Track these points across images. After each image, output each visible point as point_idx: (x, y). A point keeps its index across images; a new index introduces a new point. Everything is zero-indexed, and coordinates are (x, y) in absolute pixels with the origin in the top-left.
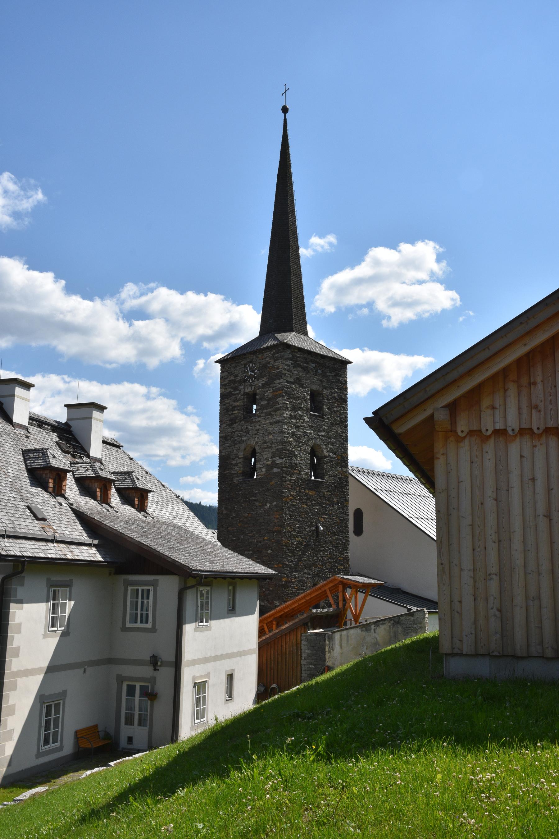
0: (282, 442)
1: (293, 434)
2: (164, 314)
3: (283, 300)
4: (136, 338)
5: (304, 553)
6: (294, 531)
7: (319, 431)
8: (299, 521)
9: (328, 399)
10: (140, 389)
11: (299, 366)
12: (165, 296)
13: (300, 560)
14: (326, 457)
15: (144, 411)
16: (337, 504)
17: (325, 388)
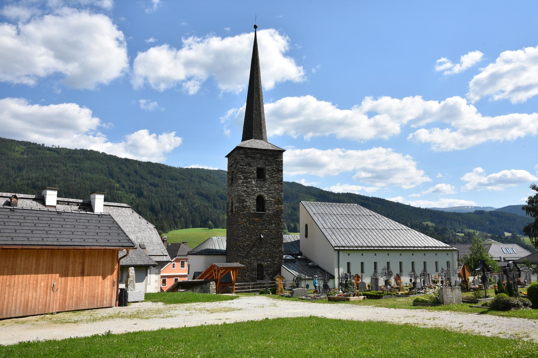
0: (238, 196)
1: (245, 191)
2: (388, 111)
3: (253, 124)
4: (376, 125)
5: (251, 249)
6: (245, 238)
7: (263, 188)
8: (248, 234)
9: (269, 171)
10: (381, 150)
11: (249, 156)
12: (386, 101)
13: (248, 252)
14: (267, 201)
15: (386, 161)
16: (275, 223)
17: (267, 166)
